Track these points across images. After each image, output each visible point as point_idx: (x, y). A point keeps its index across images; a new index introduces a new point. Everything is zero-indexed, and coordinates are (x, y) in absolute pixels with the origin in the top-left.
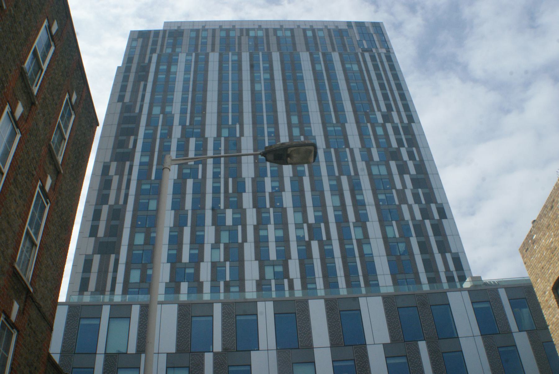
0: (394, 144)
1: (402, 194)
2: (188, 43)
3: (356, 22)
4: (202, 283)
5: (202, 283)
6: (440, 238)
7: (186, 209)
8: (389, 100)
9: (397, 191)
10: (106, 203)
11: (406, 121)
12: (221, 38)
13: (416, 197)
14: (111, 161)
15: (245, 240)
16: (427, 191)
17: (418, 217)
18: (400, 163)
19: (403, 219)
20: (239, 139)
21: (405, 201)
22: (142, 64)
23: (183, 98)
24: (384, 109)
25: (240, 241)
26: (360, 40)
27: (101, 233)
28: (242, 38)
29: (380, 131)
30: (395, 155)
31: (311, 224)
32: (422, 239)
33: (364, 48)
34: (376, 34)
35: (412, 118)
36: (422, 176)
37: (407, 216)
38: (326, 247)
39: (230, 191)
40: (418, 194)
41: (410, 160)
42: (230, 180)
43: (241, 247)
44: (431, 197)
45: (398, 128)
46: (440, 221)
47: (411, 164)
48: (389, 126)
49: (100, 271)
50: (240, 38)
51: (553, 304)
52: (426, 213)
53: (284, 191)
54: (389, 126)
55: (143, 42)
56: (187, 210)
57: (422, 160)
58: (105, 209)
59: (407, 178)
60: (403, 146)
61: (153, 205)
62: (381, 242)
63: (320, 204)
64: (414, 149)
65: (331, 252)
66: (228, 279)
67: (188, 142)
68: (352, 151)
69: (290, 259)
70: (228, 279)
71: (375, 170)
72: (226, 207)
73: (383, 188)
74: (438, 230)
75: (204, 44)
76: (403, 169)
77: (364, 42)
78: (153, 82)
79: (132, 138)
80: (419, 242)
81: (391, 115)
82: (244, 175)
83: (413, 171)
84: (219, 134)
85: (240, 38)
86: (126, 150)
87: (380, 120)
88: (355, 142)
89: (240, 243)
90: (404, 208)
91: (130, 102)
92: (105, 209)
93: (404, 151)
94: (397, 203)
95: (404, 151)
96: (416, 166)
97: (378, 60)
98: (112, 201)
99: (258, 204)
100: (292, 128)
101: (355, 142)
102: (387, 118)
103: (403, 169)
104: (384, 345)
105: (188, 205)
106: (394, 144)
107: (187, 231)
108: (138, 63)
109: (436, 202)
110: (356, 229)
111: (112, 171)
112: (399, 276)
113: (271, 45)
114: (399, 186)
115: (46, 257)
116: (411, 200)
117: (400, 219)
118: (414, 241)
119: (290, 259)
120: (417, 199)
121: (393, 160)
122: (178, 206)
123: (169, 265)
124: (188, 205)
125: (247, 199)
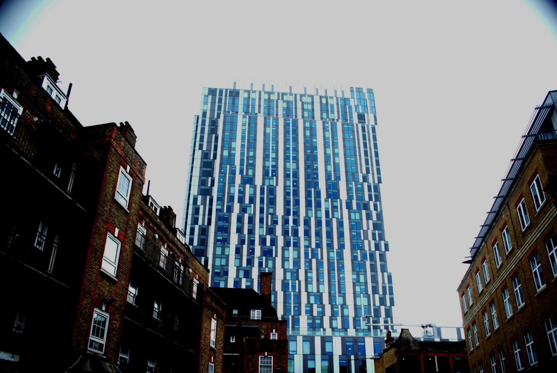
0: (367, 199)
1: (366, 233)
2: (243, 104)
4: (253, 279)
5: (253, 279)
6: (383, 263)
7: (244, 234)
9: (364, 231)
10: (197, 224)
11: (376, 182)
12: (265, 100)
13: (374, 235)
14: (198, 195)
16: (381, 232)
17: (373, 249)
18: (368, 212)
19: (364, 250)
20: (276, 187)
22: (213, 119)
24: (364, 172)
26: (357, 105)
28: (279, 101)
32: (373, 263)
33: (359, 112)
34: (369, 100)
36: (379, 222)
37: (367, 248)
39: (269, 224)
40: (375, 234)
41: (375, 210)
44: (382, 237)
45: (371, 186)
46: (385, 252)
47: (374, 213)
48: (365, 184)
50: (277, 101)
51: (26, 150)
52: (377, 247)
55: (212, 98)
56: (245, 235)
57: (381, 211)
58: (197, 228)
59: (371, 222)
64: (378, 203)
69: (300, 269)
71: (353, 217)
73: (355, 229)
74: (383, 257)
75: (254, 107)
76: (369, 217)
77: (360, 107)
79: (210, 179)
80: (371, 265)
83: (375, 218)
84: (264, 184)
85: (277, 101)
86: (206, 188)
87: (361, 180)
88: (343, 195)
89: (274, 257)
90: (366, 242)
91: (207, 150)
92: (197, 228)
93: (372, 204)
94: (362, 239)
95: (372, 204)
98: (200, 223)
99: (285, 233)
100: (355, 286)
101: (343, 195)
102: (365, 179)
103: (369, 217)
104: (339, 356)
105: (246, 232)
106: (367, 199)
107: (245, 247)
108: (210, 118)
109: (384, 240)
110: (273, 153)
113: (298, 109)
114: (365, 228)
115: (92, 250)
117: (362, 249)
118: (368, 263)
119: (300, 269)
120: (374, 238)
121: (364, 210)
122: (239, 230)
124: (246, 232)
125: (279, 230)
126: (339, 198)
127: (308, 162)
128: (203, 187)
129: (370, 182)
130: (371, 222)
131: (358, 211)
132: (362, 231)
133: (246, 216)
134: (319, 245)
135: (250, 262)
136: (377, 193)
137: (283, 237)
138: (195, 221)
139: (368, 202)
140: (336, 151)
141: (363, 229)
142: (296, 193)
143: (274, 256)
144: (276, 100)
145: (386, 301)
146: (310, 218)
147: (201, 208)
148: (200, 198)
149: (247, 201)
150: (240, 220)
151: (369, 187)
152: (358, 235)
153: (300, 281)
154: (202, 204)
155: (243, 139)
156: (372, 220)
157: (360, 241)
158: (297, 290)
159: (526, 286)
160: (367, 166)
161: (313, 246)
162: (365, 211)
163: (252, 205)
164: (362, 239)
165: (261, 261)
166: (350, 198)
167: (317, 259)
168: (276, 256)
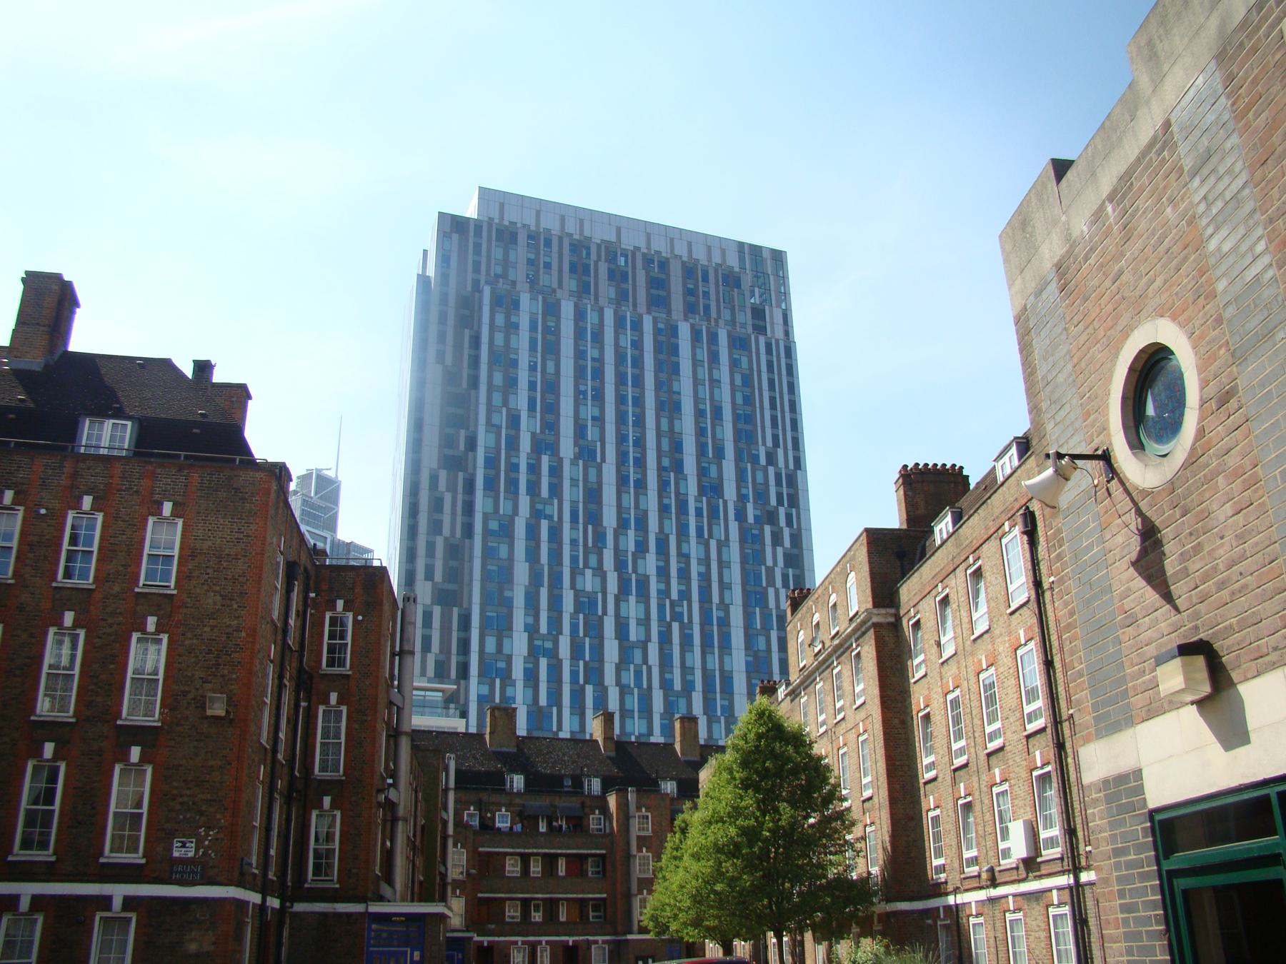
0: (773, 502)
1: (770, 572)
3: (751, 246)
8: (772, 354)
10: (440, 533)
11: (791, 466)
13: (785, 578)
15: (605, 613)
16: (798, 572)
18: (776, 529)
21: (773, 585)
23: (530, 382)
24: (769, 443)
25: (600, 613)
27: (438, 577)
29: (760, 476)
30: (771, 518)
31: (674, 600)
35: (799, 463)
36: (795, 551)
37: (772, 604)
38: (686, 631)
39: (590, 544)
42: (590, 527)
43: (601, 620)
48: (771, 470)
49: (442, 627)
53: (648, 552)
54: (771, 470)
57: (799, 529)
60: (783, 505)
61: (503, 551)
62: (614, 510)
63: (684, 574)
65: (691, 636)
66: (587, 658)
67: (539, 460)
68: (725, 503)
70: (587, 658)
72: (586, 682)
78: (574, 438)
81: (777, 451)
82: (605, 524)
83: (787, 543)
87: (763, 461)
88: (730, 492)
90: (771, 591)
92: (440, 542)
93: (782, 511)
94: (764, 584)
95: (782, 511)
96: (792, 535)
97: (780, 427)
98: (446, 531)
101: (730, 492)
105: (544, 558)
106: (773, 502)
107: (544, 592)
111: (442, 486)
112: (1138, 701)
114: (769, 562)
116: (779, 583)
122: (533, 556)
123: (526, 634)
124: (544, 558)
126: (723, 497)
127: (661, 375)
128: (449, 452)
129: (780, 466)
130: (780, 550)
131: (758, 526)
132: (763, 568)
133: (544, 525)
134: (685, 595)
135: (556, 623)
136: (792, 491)
137: (617, 642)
138: (436, 527)
139: (776, 508)
140: (716, 375)
141: (765, 564)
142: (638, 362)
143: (599, 460)
144: (600, 260)
145: (783, 538)
146: (667, 536)
147: (448, 498)
148: (443, 475)
149: (545, 492)
150: (533, 533)
151: (778, 476)
152: (758, 577)
153: (651, 667)
154: (448, 490)
155: (533, 327)
156: (783, 547)
157: (758, 589)
158: (645, 686)
159: (1085, 877)
160: (772, 395)
161: (674, 596)
162: (769, 526)
163: (556, 501)
164: (764, 584)
165: (576, 668)
166: (742, 498)
167: (681, 622)
168: (603, 460)
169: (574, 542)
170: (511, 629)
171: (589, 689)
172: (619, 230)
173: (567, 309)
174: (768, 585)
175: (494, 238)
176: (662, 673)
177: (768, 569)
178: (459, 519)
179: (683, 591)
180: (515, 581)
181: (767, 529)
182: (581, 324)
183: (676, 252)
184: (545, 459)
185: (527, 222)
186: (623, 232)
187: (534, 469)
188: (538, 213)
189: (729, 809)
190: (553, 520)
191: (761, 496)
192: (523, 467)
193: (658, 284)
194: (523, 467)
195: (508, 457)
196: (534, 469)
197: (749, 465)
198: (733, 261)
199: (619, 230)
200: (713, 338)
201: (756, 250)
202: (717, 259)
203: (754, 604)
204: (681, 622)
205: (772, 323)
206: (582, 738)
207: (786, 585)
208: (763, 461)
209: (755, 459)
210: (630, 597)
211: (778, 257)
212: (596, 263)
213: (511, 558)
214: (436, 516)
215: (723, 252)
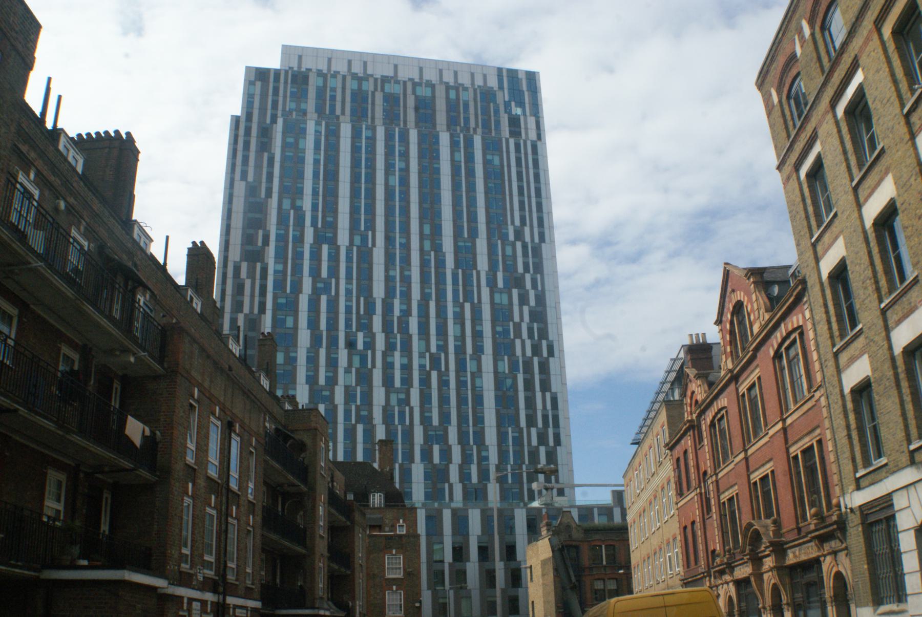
0: (520, 269)
1: (518, 327)
10: (242, 312)
11: (537, 240)
13: (531, 331)
15: (374, 366)
16: (542, 325)
24: (517, 222)
29: (509, 250)
30: (518, 282)
31: (433, 354)
36: (539, 309)
37: (519, 352)
39: (362, 312)
42: (362, 299)
43: (371, 371)
53: (411, 316)
61: (290, 322)
68: (478, 273)
82: (375, 295)
83: (532, 302)
87: (511, 237)
88: (483, 263)
90: (518, 342)
93: (528, 277)
94: (512, 337)
95: (528, 277)
98: (246, 309)
101: (483, 263)
105: (323, 326)
106: (520, 269)
111: (244, 274)
114: (517, 318)
122: (313, 324)
124: (323, 326)
128: (250, 248)
132: (511, 324)
134: (443, 348)
136: (537, 260)
139: (523, 276)
141: (512, 320)
147: (248, 283)
148: (244, 266)
152: (506, 332)
161: (433, 349)
169: (348, 310)
170: (295, 383)
171: (360, 428)
172: (396, 66)
173: (346, 130)
174: (516, 337)
175: (289, 81)
176: (422, 412)
177: (515, 324)
178: (257, 299)
179: (458, 345)
180: (299, 345)
181: (515, 292)
182: (390, 143)
183: (460, 81)
184: (325, 248)
185: (320, 68)
186: (400, 68)
187: (316, 256)
188: (330, 60)
189: (169, 523)
190: (331, 295)
191: (510, 268)
192: (307, 255)
193: (360, 103)
194: (307, 255)
195: (294, 248)
196: (316, 256)
197: (499, 242)
198: (493, 83)
199: (396, 66)
200: (469, 143)
201: (513, 74)
202: (479, 82)
203: (503, 354)
204: (439, 371)
205: (526, 129)
206: (859, 468)
207: (531, 336)
208: (511, 237)
209: (504, 237)
210: (395, 353)
211: (532, 77)
212: (373, 94)
213: (296, 328)
214: (239, 298)
215: (485, 76)
